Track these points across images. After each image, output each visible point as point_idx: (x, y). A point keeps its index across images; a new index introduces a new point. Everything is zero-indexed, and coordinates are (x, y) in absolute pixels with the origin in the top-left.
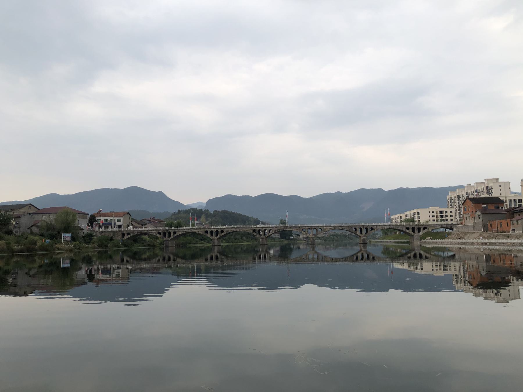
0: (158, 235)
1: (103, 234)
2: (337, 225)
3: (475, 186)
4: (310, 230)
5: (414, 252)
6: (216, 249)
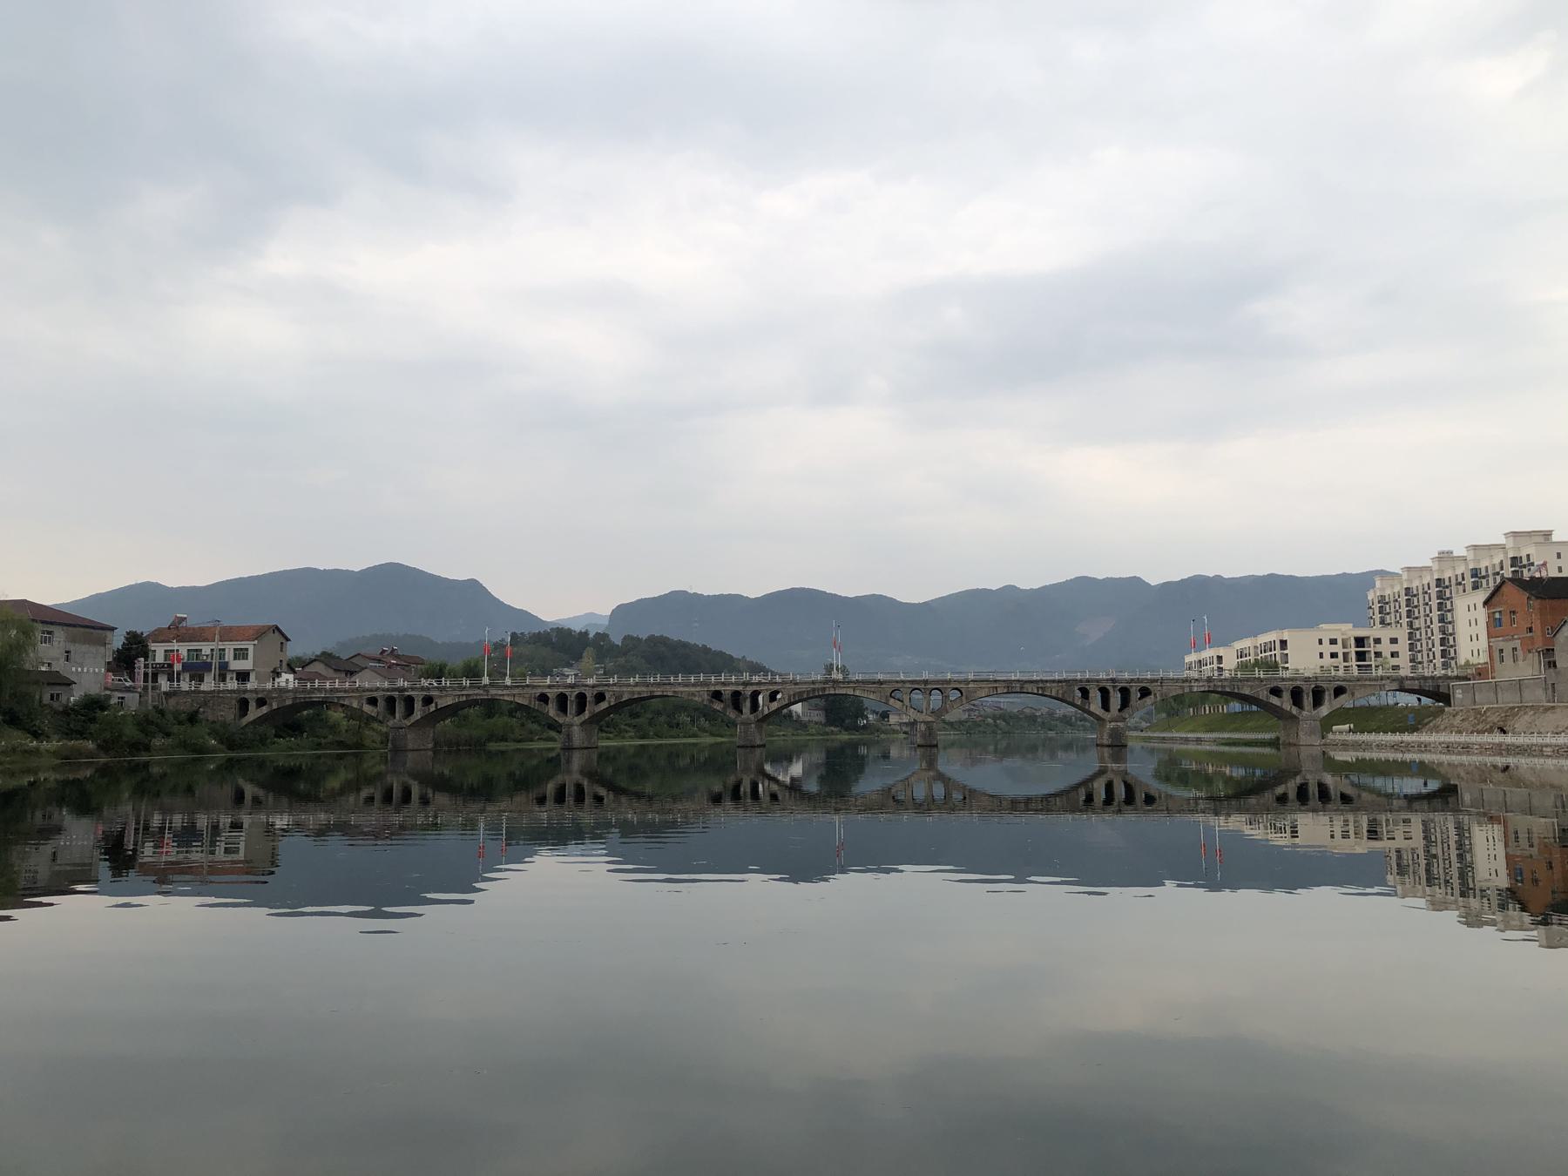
0: (367, 708)
1: (172, 701)
3: (1405, 577)
5: (1299, 780)
6: (577, 761)
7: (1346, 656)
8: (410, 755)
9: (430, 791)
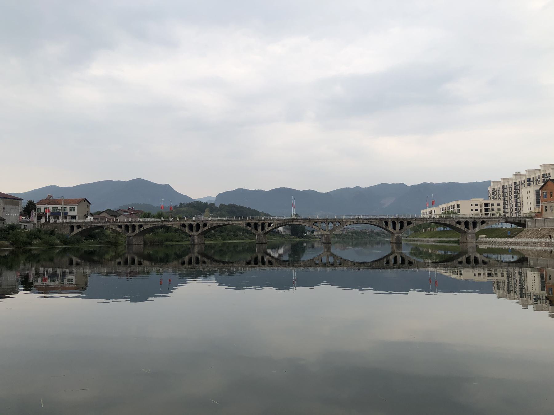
0: (118, 229)
1: (46, 226)
3: (502, 182)
4: (324, 225)
5: (467, 256)
6: (196, 249)
7: (481, 210)
9: (142, 260)
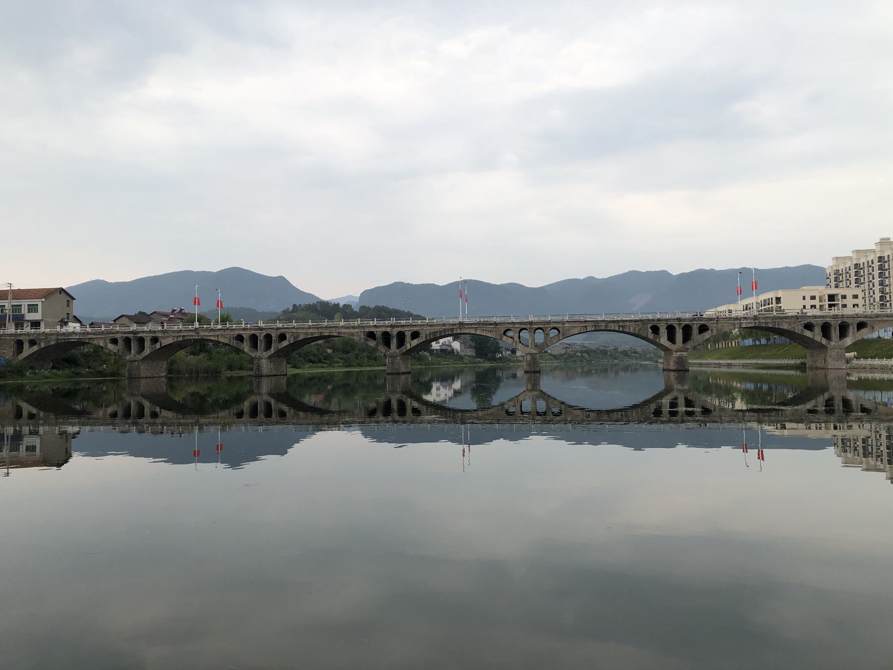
0: (111, 346)
2: (603, 318)
6: (266, 386)
8: (143, 381)
